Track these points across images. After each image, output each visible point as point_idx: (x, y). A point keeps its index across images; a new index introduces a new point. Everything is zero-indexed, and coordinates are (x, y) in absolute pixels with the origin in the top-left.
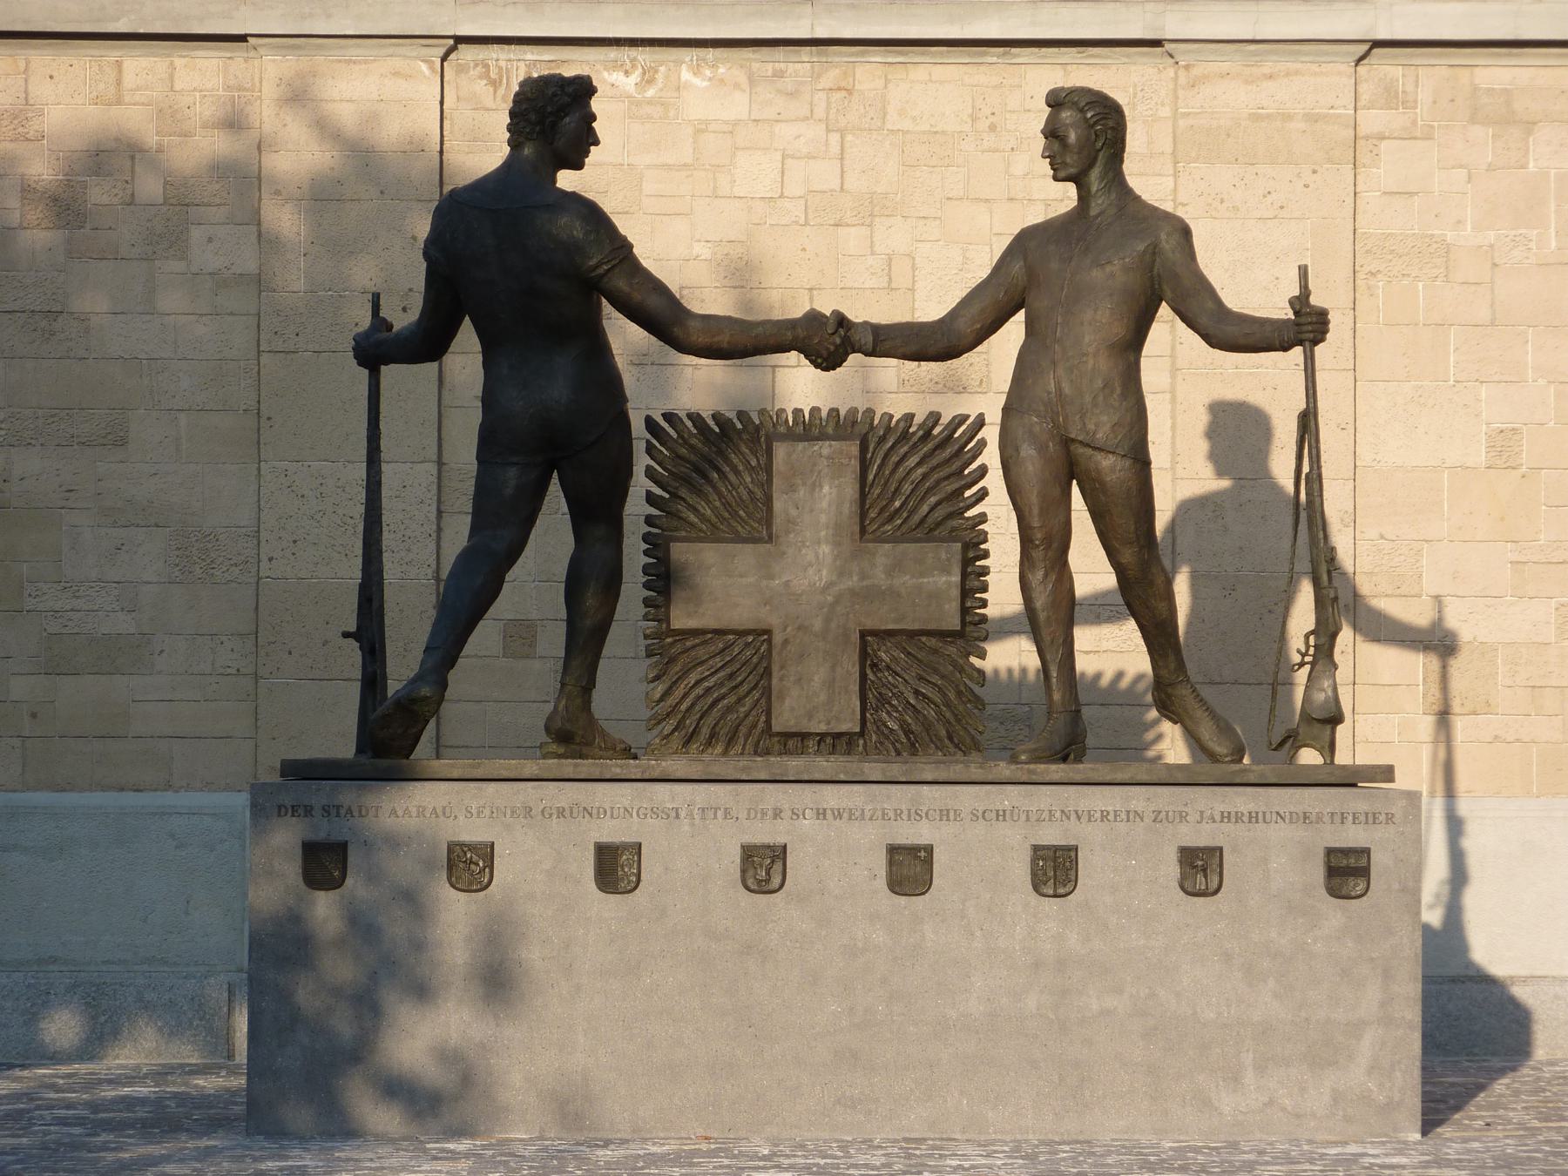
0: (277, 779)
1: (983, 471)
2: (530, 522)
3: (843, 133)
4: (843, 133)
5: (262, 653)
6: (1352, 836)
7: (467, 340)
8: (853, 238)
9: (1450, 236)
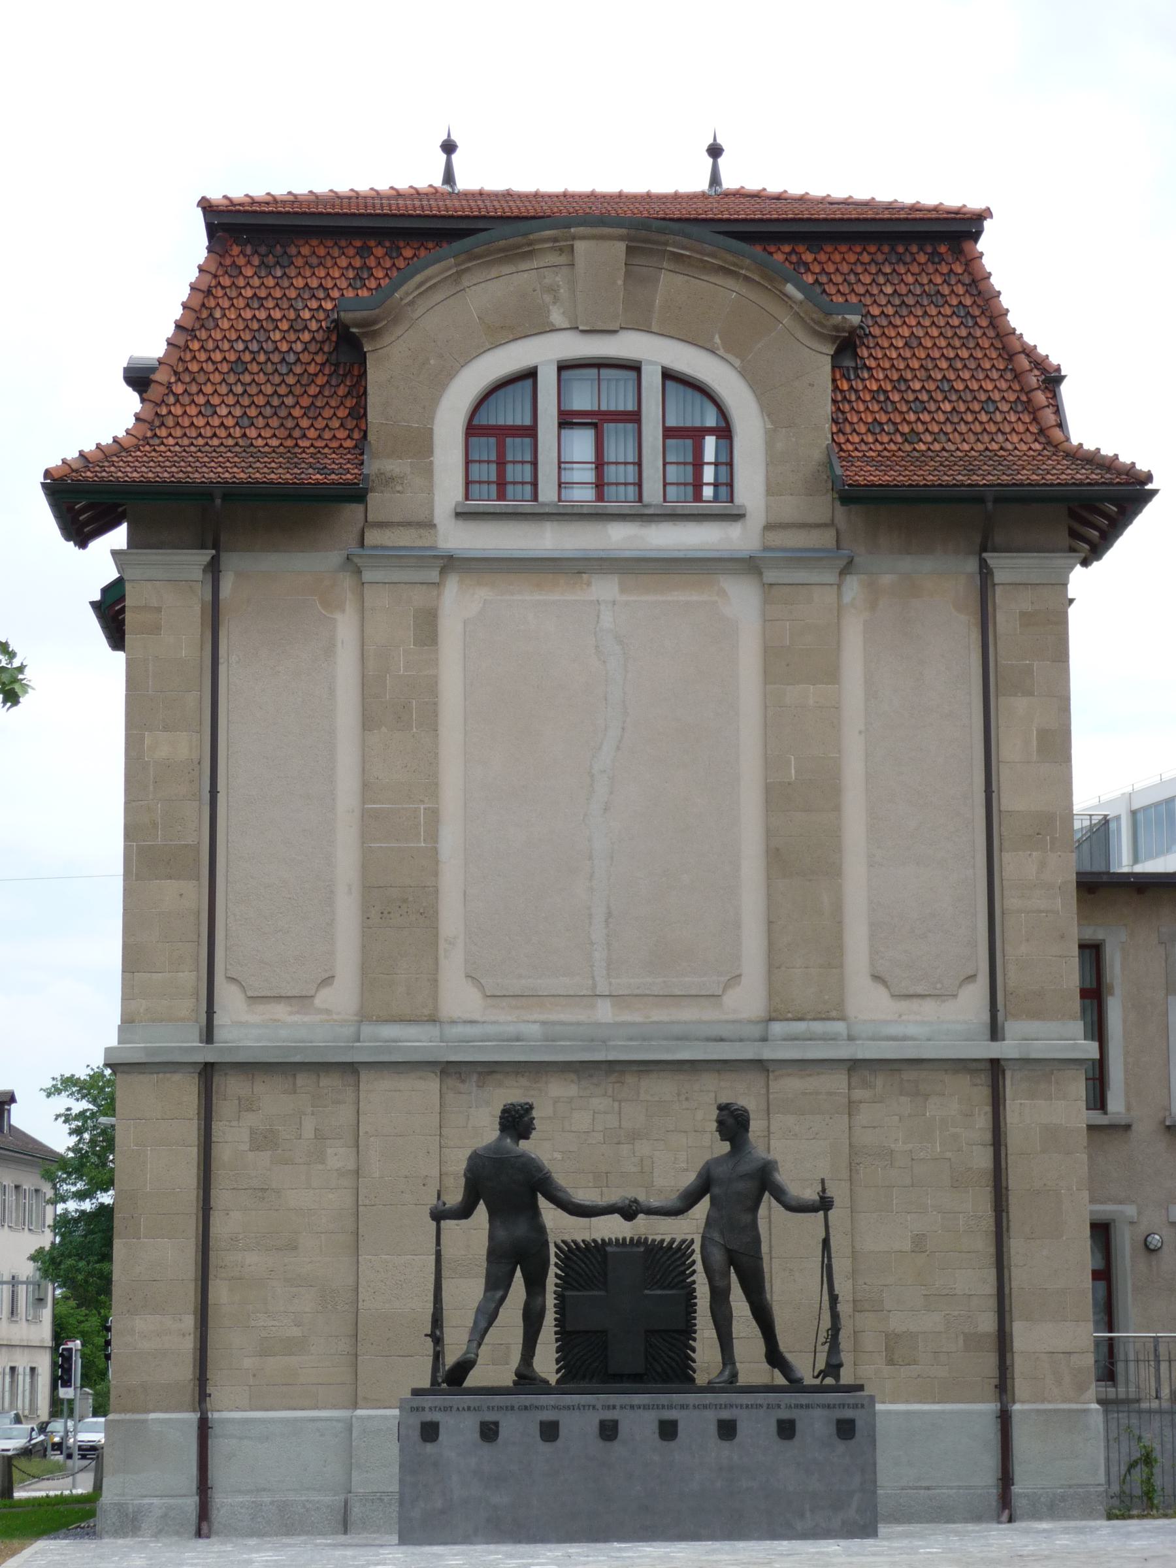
0: (409, 1396)
1: (694, 1262)
2: (509, 1286)
3: (620, 1101)
4: (620, 1101)
5: (359, 1344)
6: (848, 1414)
7: (481, 1211)
8: (625, 1149)
9: (893, 1146)
